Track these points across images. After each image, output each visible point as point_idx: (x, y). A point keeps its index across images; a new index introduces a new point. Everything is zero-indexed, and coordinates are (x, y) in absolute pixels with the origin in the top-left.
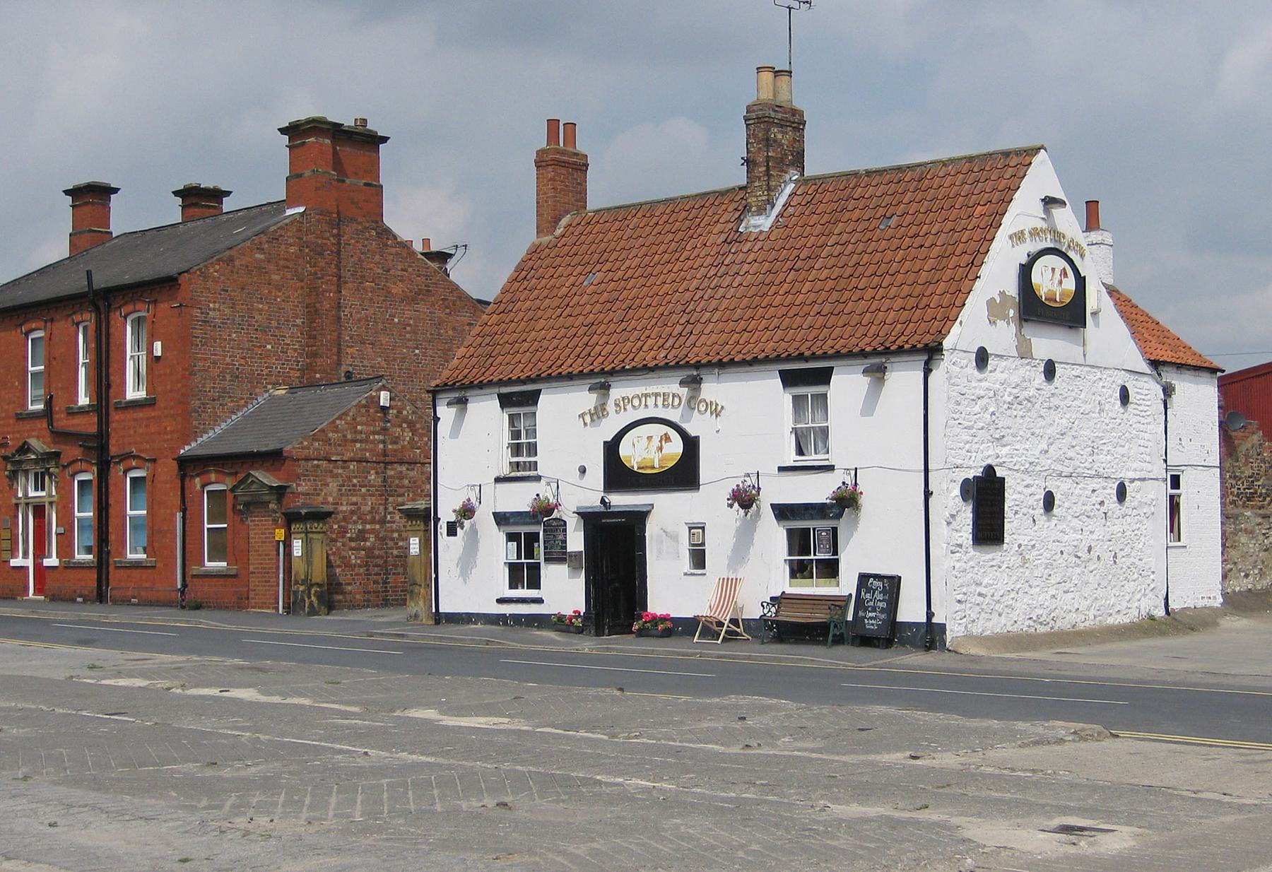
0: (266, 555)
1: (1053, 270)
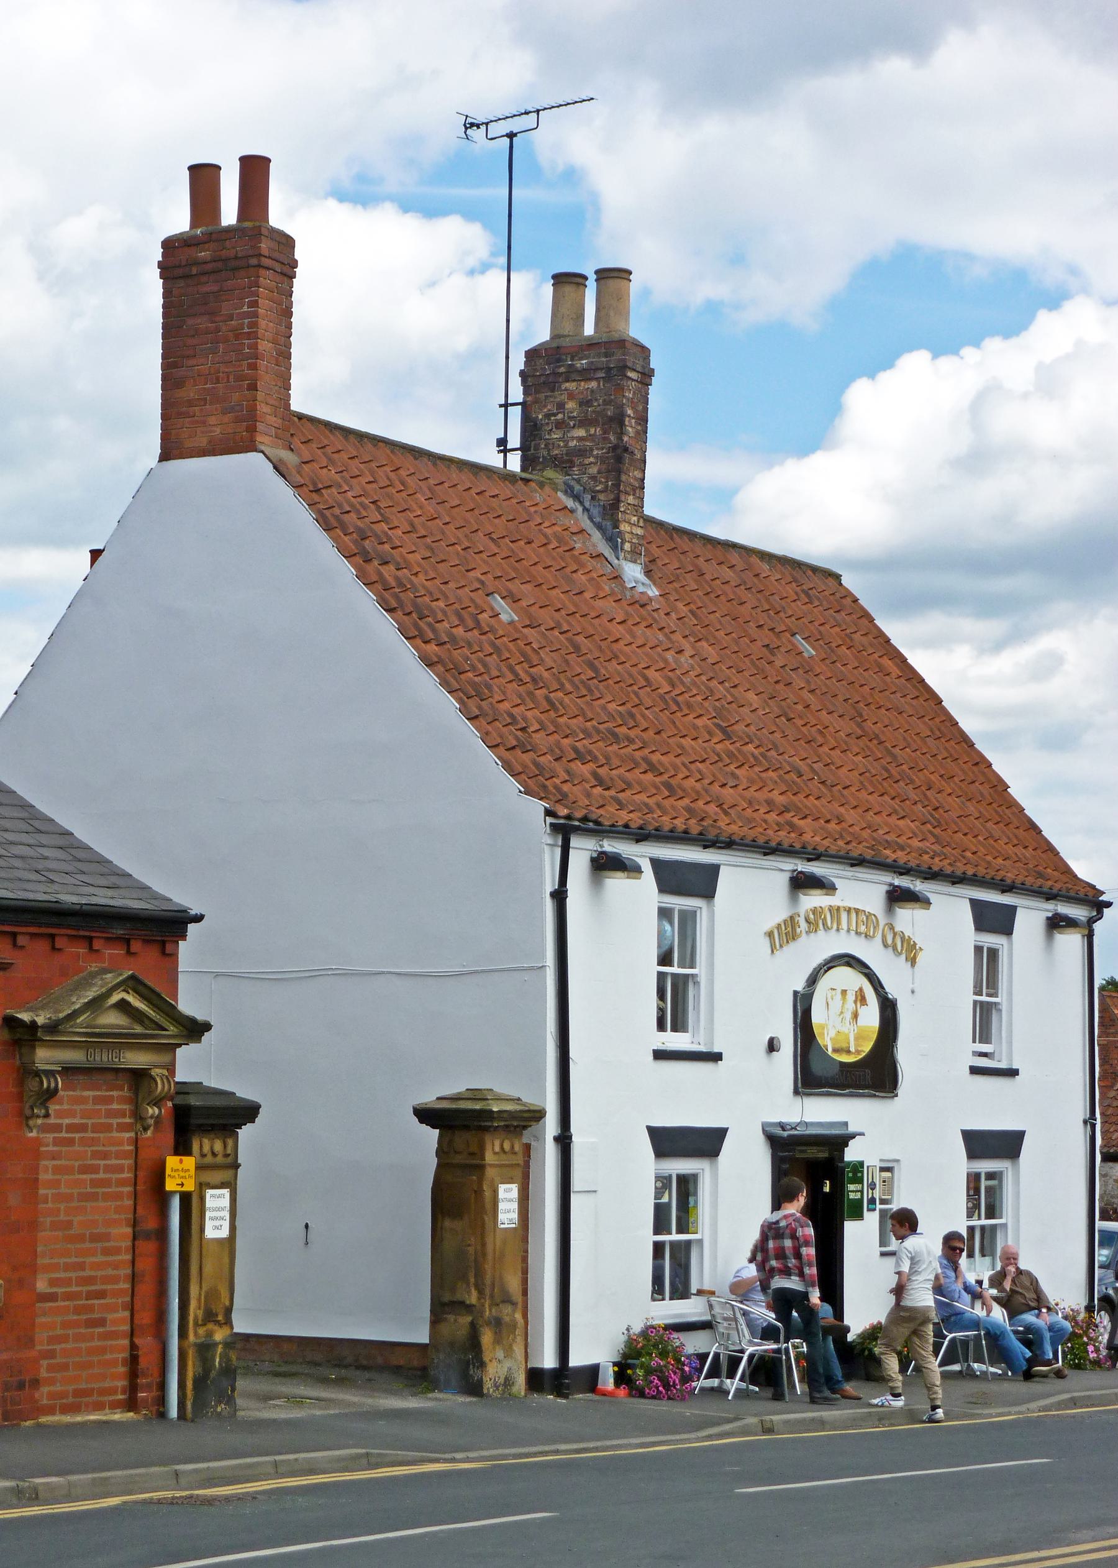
0: (95, 1238)
1: (844, 992)
